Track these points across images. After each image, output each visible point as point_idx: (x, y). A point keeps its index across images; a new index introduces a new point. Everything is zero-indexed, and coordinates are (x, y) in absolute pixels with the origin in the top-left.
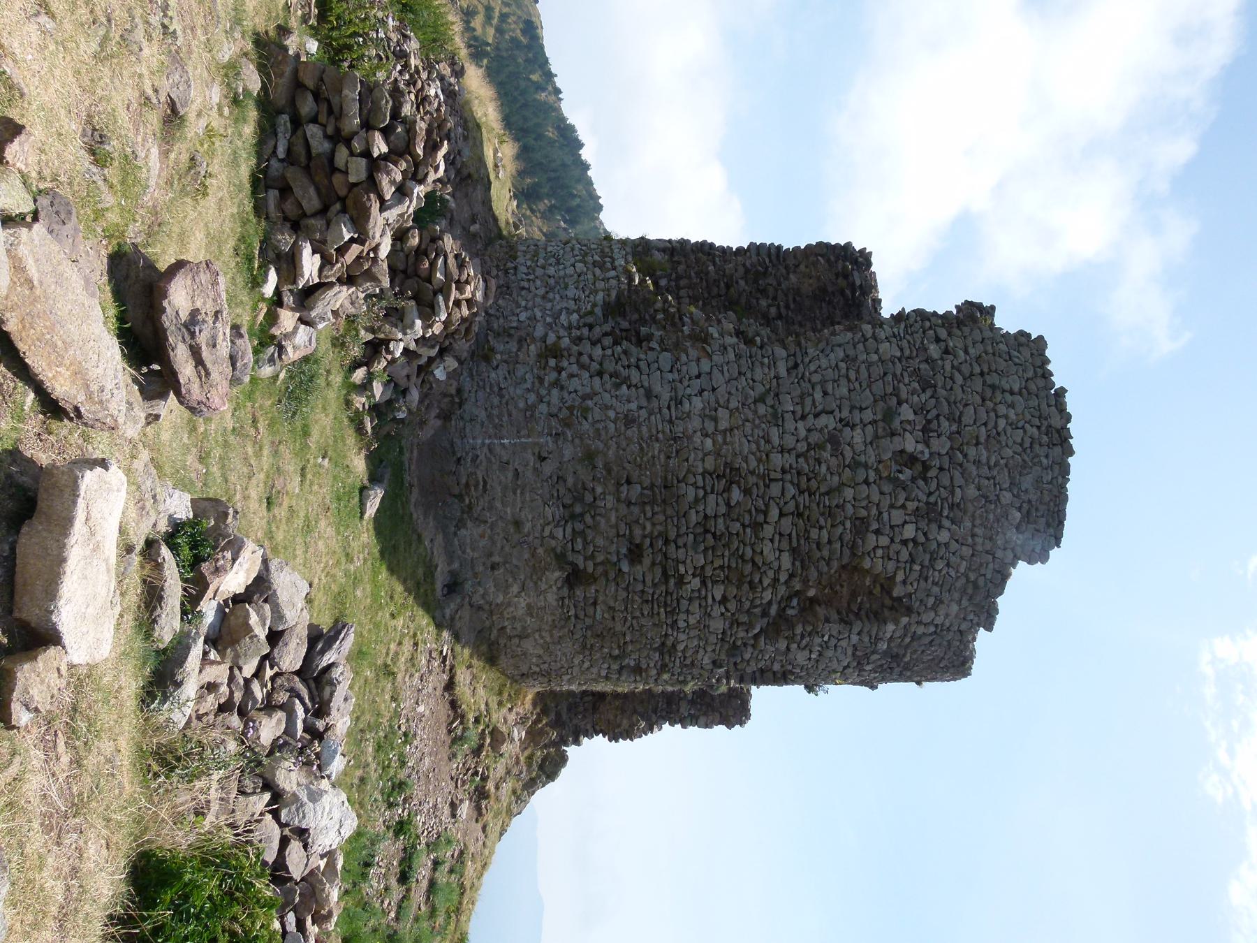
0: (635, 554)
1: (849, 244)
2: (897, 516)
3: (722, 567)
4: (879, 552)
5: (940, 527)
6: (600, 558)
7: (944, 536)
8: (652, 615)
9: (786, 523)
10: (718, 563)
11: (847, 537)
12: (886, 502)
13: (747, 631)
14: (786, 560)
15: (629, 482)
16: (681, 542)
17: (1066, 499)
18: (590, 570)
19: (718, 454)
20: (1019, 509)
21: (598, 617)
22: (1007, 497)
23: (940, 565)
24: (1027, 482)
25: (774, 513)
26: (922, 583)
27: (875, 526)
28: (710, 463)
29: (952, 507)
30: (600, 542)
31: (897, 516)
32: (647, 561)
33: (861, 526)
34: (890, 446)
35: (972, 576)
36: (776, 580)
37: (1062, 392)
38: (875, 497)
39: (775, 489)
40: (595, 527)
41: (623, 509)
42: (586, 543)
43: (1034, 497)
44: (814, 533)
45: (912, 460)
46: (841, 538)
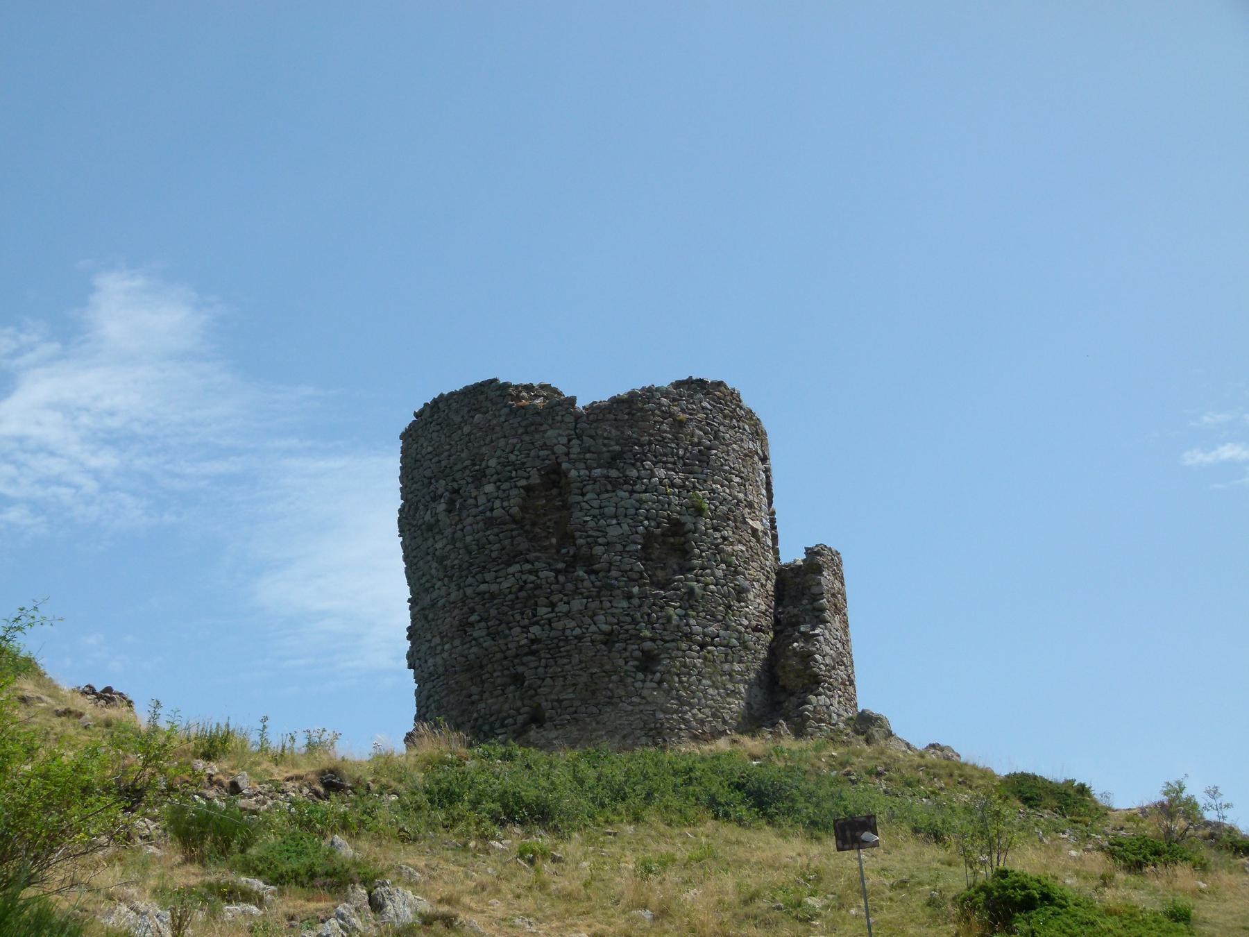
0: (518, 679)
1: (409, 601)
2: (482, 500)
3: (522, 613)
4: (505, 504)
5: (488, 467)
6: (519, 703)
7: (493, 462)
8: (569, 656)
9: (489, 576)
10: (518, 617)
11: (496, 530)
12: (473, 511)
13: (583, 581)
14: (515, 568)
15: (470, 696)
16: (504, 648)
17: (466, 388)
18: (526, 709)
19: (453, 638)
20: (473, 417)
21: (571, 696)
22: (466, 429)
23: (512, 457)
24: (457, 419)
25: (483, 587)
26: (528, 465)
27: (488, 514)
28: (457, 642)
29: (474, 465)
30: (506, 706)
31: (482, 500)
32: (520, 669)
33: (490, 523)
34: (445, 520)
35: (520, 431)
36: (530, 572)
37: (415, 414)
38: (470, 520)
39: (469, 591)
40: (499, 712)
41: (486, 695)
42: (509, 716)
43: (466, 410)
44: (494, 555)
45: (451, 502)
46: (497, 535)
